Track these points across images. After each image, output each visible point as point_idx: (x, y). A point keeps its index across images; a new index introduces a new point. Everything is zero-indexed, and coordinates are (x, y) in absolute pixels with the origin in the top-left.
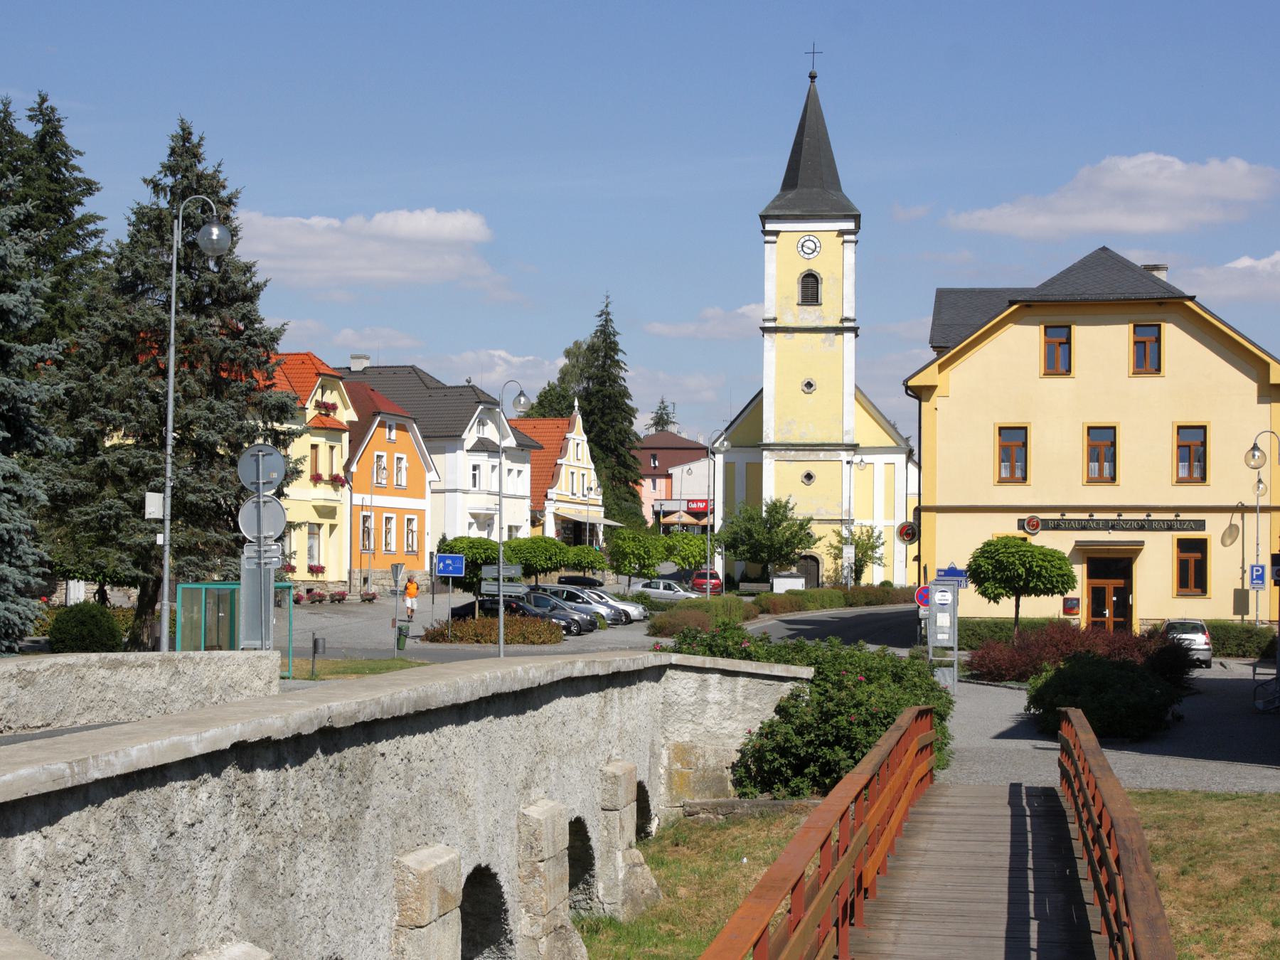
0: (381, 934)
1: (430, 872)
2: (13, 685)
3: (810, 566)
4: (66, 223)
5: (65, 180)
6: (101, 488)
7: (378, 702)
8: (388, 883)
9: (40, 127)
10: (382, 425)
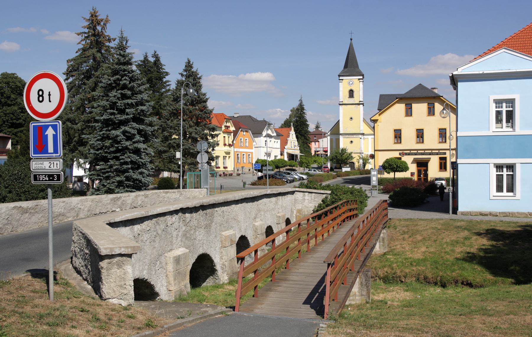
0: (217, 249)
1: (228, 236)
2: (143, 197)
3: (352, 165)
4: (161, 83)
5: (161, 72)
6: (170, 149)
7: (214, 200)
8: (218, 238)
9: (155, 59)
10: (241, 131)
